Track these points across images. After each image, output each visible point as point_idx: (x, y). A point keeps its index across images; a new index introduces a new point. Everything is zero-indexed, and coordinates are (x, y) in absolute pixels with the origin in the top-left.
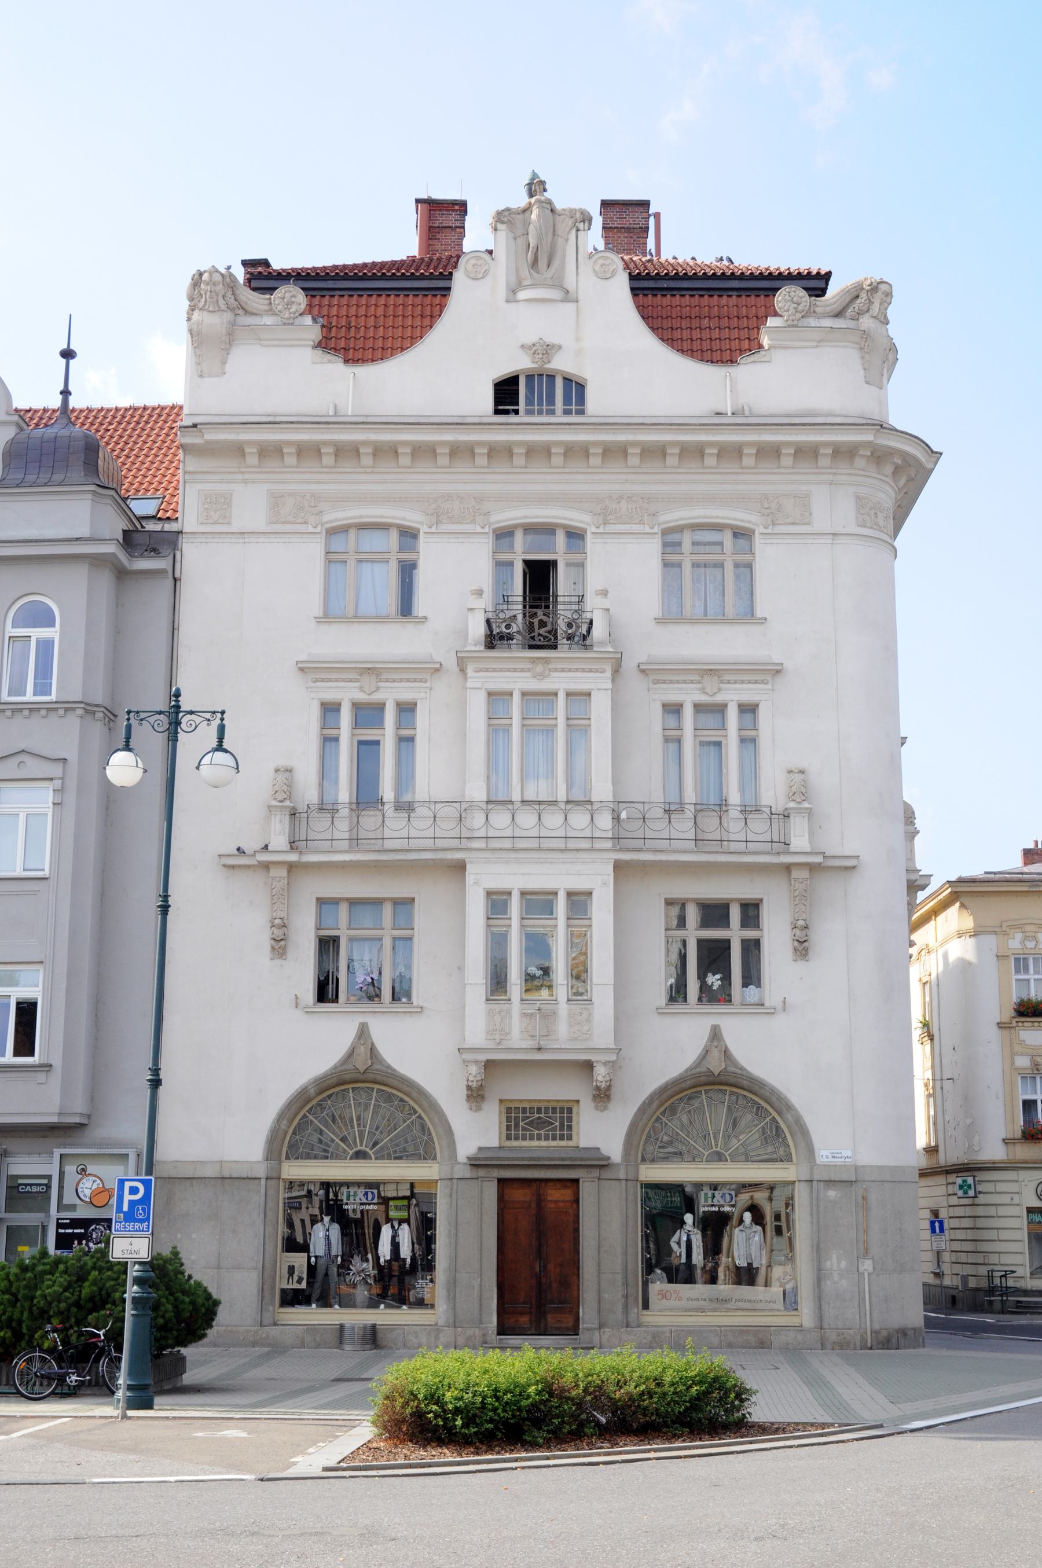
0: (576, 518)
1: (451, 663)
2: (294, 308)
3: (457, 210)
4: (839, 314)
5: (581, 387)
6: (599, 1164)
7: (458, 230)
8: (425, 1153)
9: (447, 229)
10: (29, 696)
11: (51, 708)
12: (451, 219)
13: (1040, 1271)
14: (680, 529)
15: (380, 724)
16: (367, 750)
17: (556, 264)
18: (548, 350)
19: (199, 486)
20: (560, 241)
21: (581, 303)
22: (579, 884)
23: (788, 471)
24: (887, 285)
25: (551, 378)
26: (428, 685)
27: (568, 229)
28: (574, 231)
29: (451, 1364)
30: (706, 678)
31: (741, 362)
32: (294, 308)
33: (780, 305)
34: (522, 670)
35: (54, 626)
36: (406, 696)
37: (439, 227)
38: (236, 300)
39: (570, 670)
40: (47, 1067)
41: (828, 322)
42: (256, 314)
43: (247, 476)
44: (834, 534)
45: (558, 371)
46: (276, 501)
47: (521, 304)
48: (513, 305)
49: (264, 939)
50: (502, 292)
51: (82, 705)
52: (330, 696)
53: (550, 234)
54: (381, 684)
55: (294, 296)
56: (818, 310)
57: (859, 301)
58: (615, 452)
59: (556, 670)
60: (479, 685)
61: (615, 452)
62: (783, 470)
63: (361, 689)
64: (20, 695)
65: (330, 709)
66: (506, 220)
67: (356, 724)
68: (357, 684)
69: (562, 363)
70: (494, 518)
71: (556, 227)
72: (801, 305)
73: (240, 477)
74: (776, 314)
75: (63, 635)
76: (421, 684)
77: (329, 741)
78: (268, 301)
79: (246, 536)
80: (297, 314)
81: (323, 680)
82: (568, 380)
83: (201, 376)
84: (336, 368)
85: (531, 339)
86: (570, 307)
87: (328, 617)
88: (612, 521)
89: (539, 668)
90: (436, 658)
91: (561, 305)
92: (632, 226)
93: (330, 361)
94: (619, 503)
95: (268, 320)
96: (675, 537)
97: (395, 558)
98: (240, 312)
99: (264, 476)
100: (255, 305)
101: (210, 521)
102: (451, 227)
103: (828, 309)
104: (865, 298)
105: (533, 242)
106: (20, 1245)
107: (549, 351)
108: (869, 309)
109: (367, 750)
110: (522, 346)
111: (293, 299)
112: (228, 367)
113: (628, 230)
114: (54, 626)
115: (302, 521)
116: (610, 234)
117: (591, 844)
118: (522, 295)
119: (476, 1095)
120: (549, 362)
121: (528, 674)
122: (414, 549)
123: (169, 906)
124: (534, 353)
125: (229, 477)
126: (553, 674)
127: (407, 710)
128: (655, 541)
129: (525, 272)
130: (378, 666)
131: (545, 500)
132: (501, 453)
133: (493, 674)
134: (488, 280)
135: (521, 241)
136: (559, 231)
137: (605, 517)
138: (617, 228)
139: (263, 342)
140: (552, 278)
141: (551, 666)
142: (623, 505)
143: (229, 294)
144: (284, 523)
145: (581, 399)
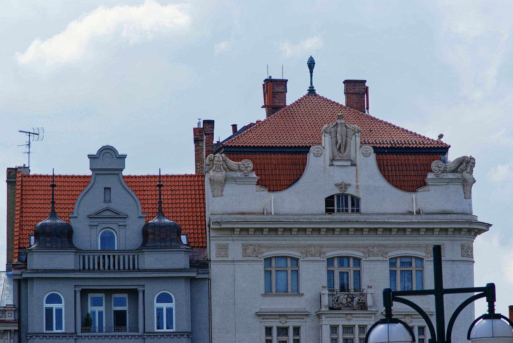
0: (358, 254)
2: (249, 169)
3: (283, 84)
4: (455, 171)
5: (358, 200)
7: (284, 93)
9: (279, 93)
10: (165, 330)
11: (175, 334)
12: (280, 89)
14: (396, 258)
15: (287, 334)
17: (348, 149)
19: (215, 242)
20: (349, 139)
21: (359, 167)
23: (437, 236)
24: (473, 160)
25: (346, 196)
26: (305, 320)
27: (352, 134)
28: (354, 135)
30: (407, 317)
31: (419, 191)
32: (249, 169)
33: (433, 168)
34: (343, 317)
35: (172, 302)
36: (297, 324)
37: (276, 92)
38: (226, 165)
39: (360, 317)
41: (451, 176)
42: (233, 171)
43: (234, 238)
44: (453, 261)
45: (349, 194)
46: (245, 248)
47: (335, 167)
48: (332, 167)
50: (328, 162)
51: (187, 334)
52: (269, 325)
53: (345, 137)
54: (288, 320)
55: (249, 164)
56: (447, 169)
57: (463, 165)
59: (355, 317)
60: (327, 323)
62: (434, 236)
63: (280, 322)
64: (114, 305)
65: (269, 330)
66: (328, 132)
67: (279, 335)
68: (279, 320)
69: (351, 191)
70: (327, 255)
71: (347, 133)
72: (441, 168)
73: (231, 238)
74: (432, 171)
75: (176, 306)
76: (302, 320)
78: (238, 166)
79: (235, 262)
80: (250, 171)
81: (266, 319)
82: (353, 197)
83: (214, 197)
84: (265, 193)
85: (339, 182)
86: (354, 168)
87: (268, 292)
88: (371, 256)
89: (349, 317)
90: (308, 310)
91: (350, 167)
92: (358, 92)
93: (263, 191)
94: (374, 248)
95: (239, 174)
96: (394, 261)
97: (290, 269)
98: (228, 170)
99: (241, 238)
100: (234, 167)
101: (221, 256)
102: (281, 92)
103: (451, 169)
104: (465, 165)
105: (339, 141)
107: (347, 187)
108: (466, 169)
110: (336, 185)
111: (248, 165)
112: (224, 193)
113: (357, 94)
114: (172, 302)
115: (255, 256)
116: (349, 96)
118: (336, 163)
120: (346, 191)
121: (345, 319)
122: (297, 265)
124: (341, 188)
125: (227, 238)
126: (354, 319)
128: (387, 263)
129: (336, 153)
130: (287, 314)
131: (346, 247)
133: (332, 319)
134: (322, 156)
135: (334, 139)
136: (348, 136)
137: (369, 253)
138: (352, 93)
139: (237, 183)
140: (347, 156)
141: (352, 316)
142: (375, 249)
143: (224, 164)
144: (248, 256)
145: (358, 206)
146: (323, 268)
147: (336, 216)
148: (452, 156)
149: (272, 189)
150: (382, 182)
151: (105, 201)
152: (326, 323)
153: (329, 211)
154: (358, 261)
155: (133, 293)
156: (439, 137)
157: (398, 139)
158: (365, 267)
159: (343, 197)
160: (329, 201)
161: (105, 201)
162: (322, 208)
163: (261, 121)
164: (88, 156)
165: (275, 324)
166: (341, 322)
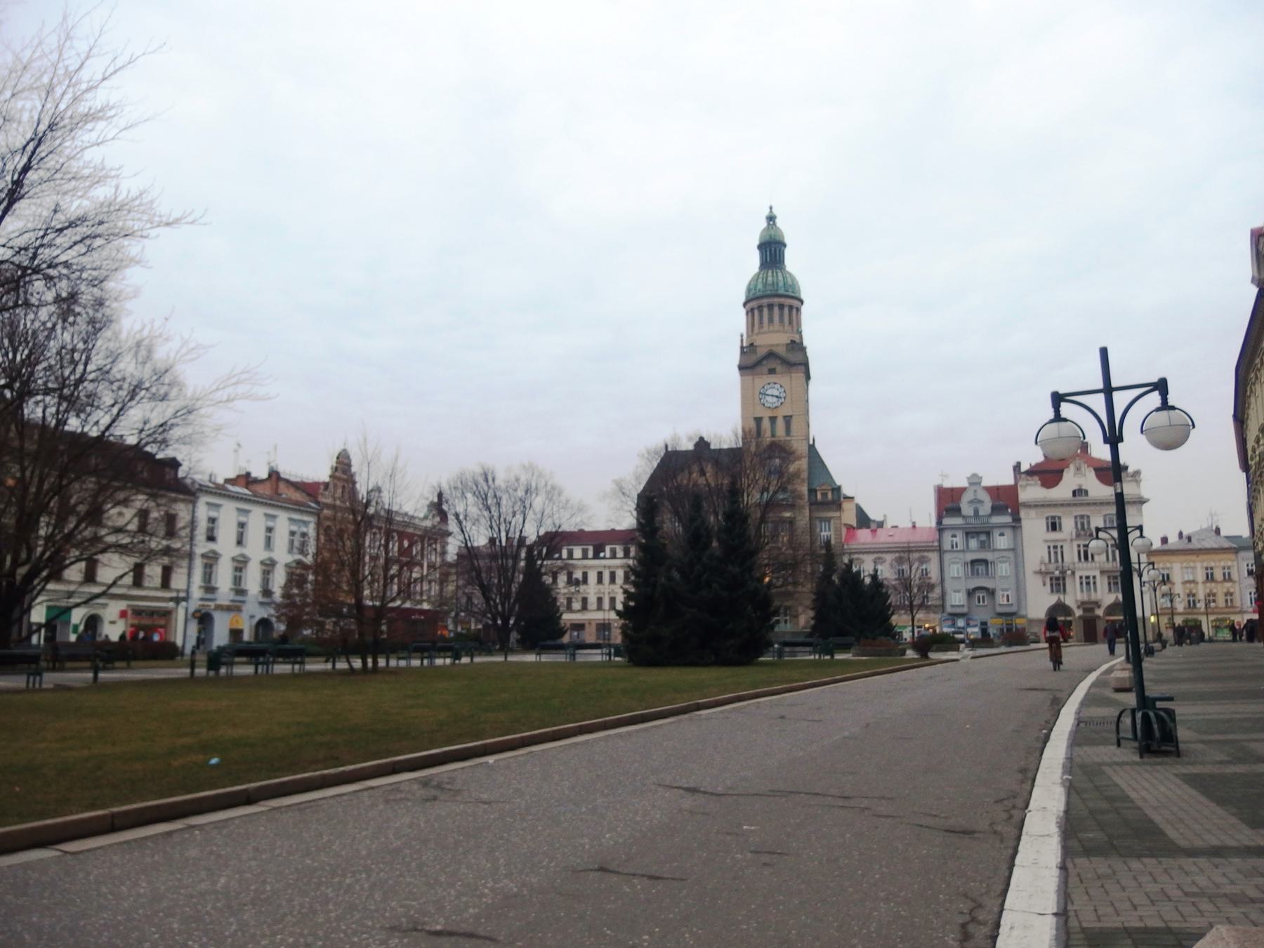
1: (1069, 540)
6: (1099, 617)
8: (1070, 615)
13: (2, 393)
16: (1056, 553)
18: (1080, 486)
22: (1094, 574)
29: (268, 888)
40: (1012, 605)
49: (1042, 584)
58: (1095, 504)
61: (1095, 504)
65: (1049, 547)
77: (1049, 553)
106: (242, 637)
109: (1056, 553)
117: (1096, 568)
119: (1079, 607)
123: (702, 444)
127: (1062, 547)
132: (1075, 505)
148: (1130, 470)
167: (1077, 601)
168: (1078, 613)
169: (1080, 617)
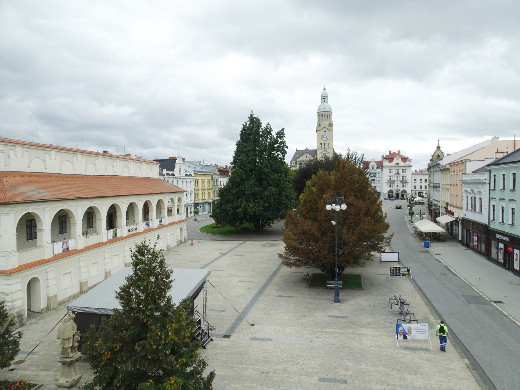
6: (399, 193)
146: (395, 170)
147: (396, 165)
148: (409, 159)
149: (390, 163)
150: (402, 162)
151: (181, 168)
152: (395, 176)
153: (396, 165)
154: (392, 170)
155: (375, 173)
156: (104, 151)
157: (405, 157)
158: (399, 170)
159: (397, 163)
160: (396, 164)
161: (181, 168)
162: (395, 164)
163: (284, 157)
164: (231, 163)
165: (390, 176)
166: (397, 176)
167: (395, 189)
168: (395, 192)
169: (395, 193)
